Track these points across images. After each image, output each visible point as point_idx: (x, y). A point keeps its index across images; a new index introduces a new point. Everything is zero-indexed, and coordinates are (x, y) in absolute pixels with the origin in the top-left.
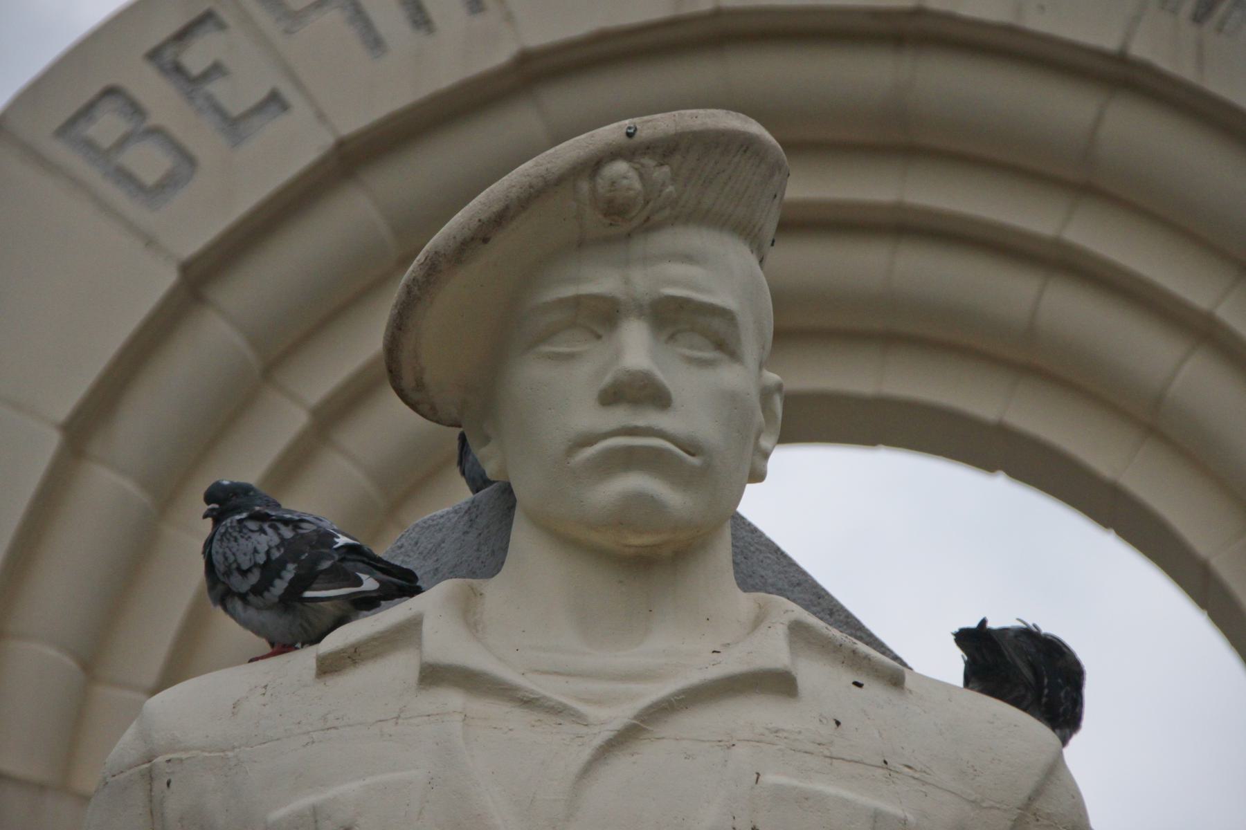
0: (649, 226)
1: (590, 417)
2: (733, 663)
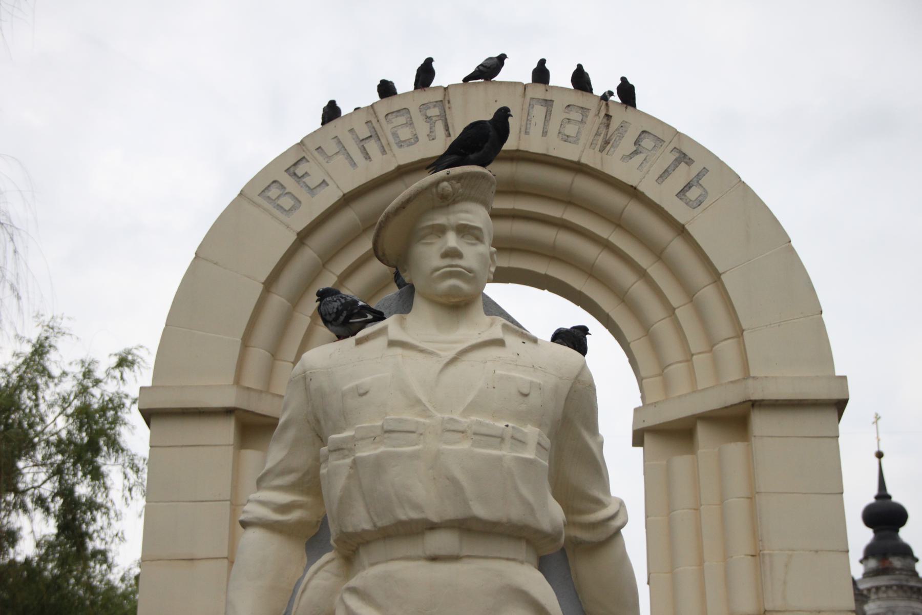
0: (454, 202)
1: (437, 262)
2: (486, 337)
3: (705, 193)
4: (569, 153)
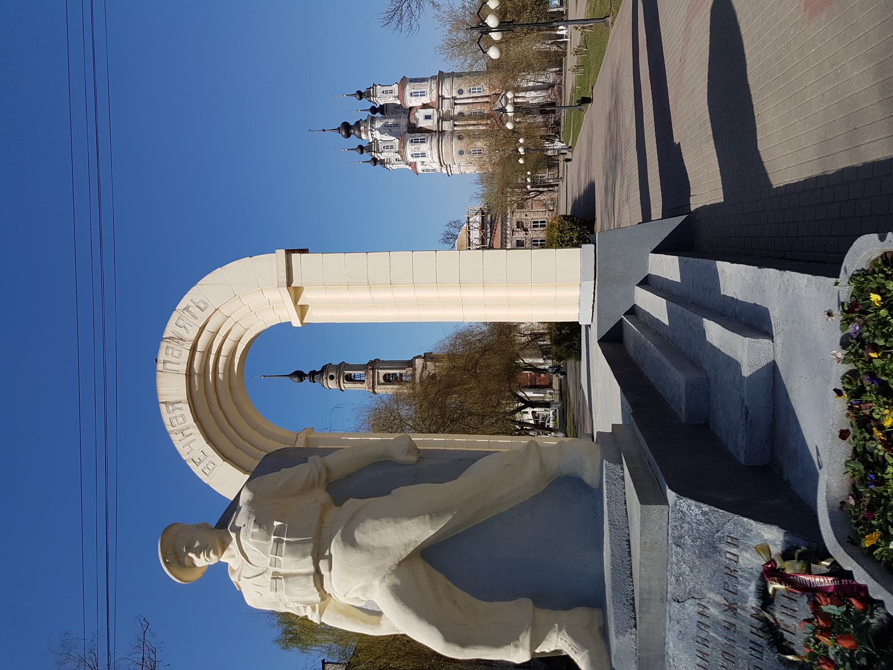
3: (202, 301)
4: (186, 354)
